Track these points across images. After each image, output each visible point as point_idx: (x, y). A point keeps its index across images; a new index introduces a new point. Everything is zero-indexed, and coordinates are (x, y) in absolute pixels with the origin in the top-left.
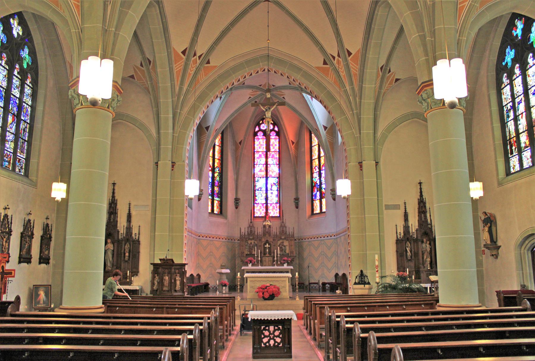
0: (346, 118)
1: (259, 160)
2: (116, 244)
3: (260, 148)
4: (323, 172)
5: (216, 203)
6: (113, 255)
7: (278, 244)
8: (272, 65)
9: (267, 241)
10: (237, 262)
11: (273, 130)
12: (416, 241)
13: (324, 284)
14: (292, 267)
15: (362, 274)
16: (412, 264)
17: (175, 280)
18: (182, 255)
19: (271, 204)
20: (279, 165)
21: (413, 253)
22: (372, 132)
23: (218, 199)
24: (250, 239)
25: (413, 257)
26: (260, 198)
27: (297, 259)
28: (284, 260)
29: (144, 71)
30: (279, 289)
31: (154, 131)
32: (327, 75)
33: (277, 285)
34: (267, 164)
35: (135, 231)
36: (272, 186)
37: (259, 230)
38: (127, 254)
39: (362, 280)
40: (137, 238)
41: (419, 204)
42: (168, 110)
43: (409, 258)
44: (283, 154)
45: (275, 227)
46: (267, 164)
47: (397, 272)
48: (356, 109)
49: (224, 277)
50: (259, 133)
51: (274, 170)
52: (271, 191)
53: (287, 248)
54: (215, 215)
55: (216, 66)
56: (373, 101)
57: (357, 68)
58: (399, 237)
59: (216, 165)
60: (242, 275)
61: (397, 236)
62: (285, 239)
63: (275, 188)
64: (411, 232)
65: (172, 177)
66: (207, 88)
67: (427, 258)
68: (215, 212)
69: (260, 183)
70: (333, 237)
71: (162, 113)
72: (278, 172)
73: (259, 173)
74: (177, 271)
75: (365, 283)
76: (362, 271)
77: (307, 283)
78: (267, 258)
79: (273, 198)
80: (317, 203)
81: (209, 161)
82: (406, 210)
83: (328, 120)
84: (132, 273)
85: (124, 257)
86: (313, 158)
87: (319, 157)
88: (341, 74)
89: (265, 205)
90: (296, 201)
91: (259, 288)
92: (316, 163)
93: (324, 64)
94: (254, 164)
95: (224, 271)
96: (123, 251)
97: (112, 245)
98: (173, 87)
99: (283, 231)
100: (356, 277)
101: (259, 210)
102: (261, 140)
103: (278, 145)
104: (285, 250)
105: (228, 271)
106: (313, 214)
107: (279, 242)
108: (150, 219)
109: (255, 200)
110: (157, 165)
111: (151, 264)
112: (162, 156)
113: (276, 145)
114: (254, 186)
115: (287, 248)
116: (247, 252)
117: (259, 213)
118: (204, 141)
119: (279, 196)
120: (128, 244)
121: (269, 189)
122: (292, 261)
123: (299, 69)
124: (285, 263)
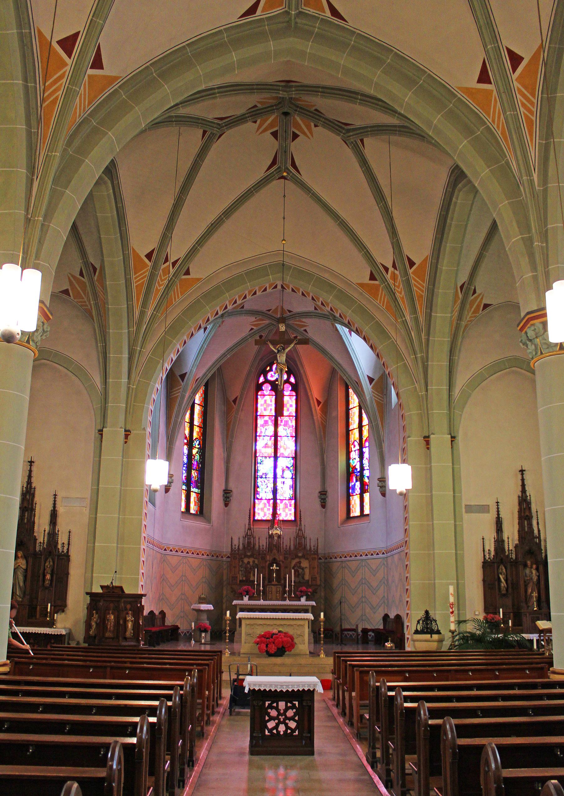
1: (263, 430)
3: (265, 410)
5: (193, 496)
6: (25, 577)
7: (293, 565)
9: (275, 559)
10: (225, 592)
12: (515, 563)
13: (365, 631)
14: (314, 603)
15: (427, 618)
16: (509, 601)
17: (125, 621)
19: (282, 500)
21: (509, 582)
22: (445, 388)
23: (196, 490)
25: (510, 590)
28: (301, 591)
30: (292, 638)
31: (97, 380)
33: (291, 632)
34: (276, 435)
35: (62, 539)
36: (283, 471)
38: (48, 577)
39: (428, 625)
40: (65, 551)
43: (504, 592)
46: (276, 435)
47: (485, 615)
48: (421, 351)
49: (204, 616)
50: (265, 385)
51: (288, 446)
52: (283, 480)
53: (307, 571)
55: (198, 280)
57: (423, 287)
58: (487, 557)
59: (195, 435)
60: (233, 615)
61: (484, 556)
62: (303, 557)
63: (288, 474)
64: (507, 549)
65: (125, 453)
67: (532, 593)
68: (192, 511)
69: (265, 467)
70: (381, 555)
72: (294, 448)
73: (264, 450)
75: (431, 632)
76: (427, 612)
78: (274, 588)
79: (285, 491)
80: (355, 500)
82: (498, 514)
84: (55, 606)
86: (351, 427)
87: (360, 427)
88: (398, 295)
89: (272, 501)
90: (323, 497)
91: (261, 636)
92: (355, 436)
93: (480, 81)
94: (256, 436)
95: (204, 607)
96: (41, 571)
97: (24, 562)
98: (130, 310)
100: (418, 622)
101: (262, 509)
102: (267, 398)
104: (304, 574)
105: (210, 607)
106: (349, 517)
107: (294, 562)
109: (256, 492)
110: (102, 435)
112: (109, 420)
114: (256, 471)
115: (307, 571)
116: (240, 577)
118: (176, 397)
119: (294, 487)
122: (315, 592)
123: (332, 287)
124: (302, 596)
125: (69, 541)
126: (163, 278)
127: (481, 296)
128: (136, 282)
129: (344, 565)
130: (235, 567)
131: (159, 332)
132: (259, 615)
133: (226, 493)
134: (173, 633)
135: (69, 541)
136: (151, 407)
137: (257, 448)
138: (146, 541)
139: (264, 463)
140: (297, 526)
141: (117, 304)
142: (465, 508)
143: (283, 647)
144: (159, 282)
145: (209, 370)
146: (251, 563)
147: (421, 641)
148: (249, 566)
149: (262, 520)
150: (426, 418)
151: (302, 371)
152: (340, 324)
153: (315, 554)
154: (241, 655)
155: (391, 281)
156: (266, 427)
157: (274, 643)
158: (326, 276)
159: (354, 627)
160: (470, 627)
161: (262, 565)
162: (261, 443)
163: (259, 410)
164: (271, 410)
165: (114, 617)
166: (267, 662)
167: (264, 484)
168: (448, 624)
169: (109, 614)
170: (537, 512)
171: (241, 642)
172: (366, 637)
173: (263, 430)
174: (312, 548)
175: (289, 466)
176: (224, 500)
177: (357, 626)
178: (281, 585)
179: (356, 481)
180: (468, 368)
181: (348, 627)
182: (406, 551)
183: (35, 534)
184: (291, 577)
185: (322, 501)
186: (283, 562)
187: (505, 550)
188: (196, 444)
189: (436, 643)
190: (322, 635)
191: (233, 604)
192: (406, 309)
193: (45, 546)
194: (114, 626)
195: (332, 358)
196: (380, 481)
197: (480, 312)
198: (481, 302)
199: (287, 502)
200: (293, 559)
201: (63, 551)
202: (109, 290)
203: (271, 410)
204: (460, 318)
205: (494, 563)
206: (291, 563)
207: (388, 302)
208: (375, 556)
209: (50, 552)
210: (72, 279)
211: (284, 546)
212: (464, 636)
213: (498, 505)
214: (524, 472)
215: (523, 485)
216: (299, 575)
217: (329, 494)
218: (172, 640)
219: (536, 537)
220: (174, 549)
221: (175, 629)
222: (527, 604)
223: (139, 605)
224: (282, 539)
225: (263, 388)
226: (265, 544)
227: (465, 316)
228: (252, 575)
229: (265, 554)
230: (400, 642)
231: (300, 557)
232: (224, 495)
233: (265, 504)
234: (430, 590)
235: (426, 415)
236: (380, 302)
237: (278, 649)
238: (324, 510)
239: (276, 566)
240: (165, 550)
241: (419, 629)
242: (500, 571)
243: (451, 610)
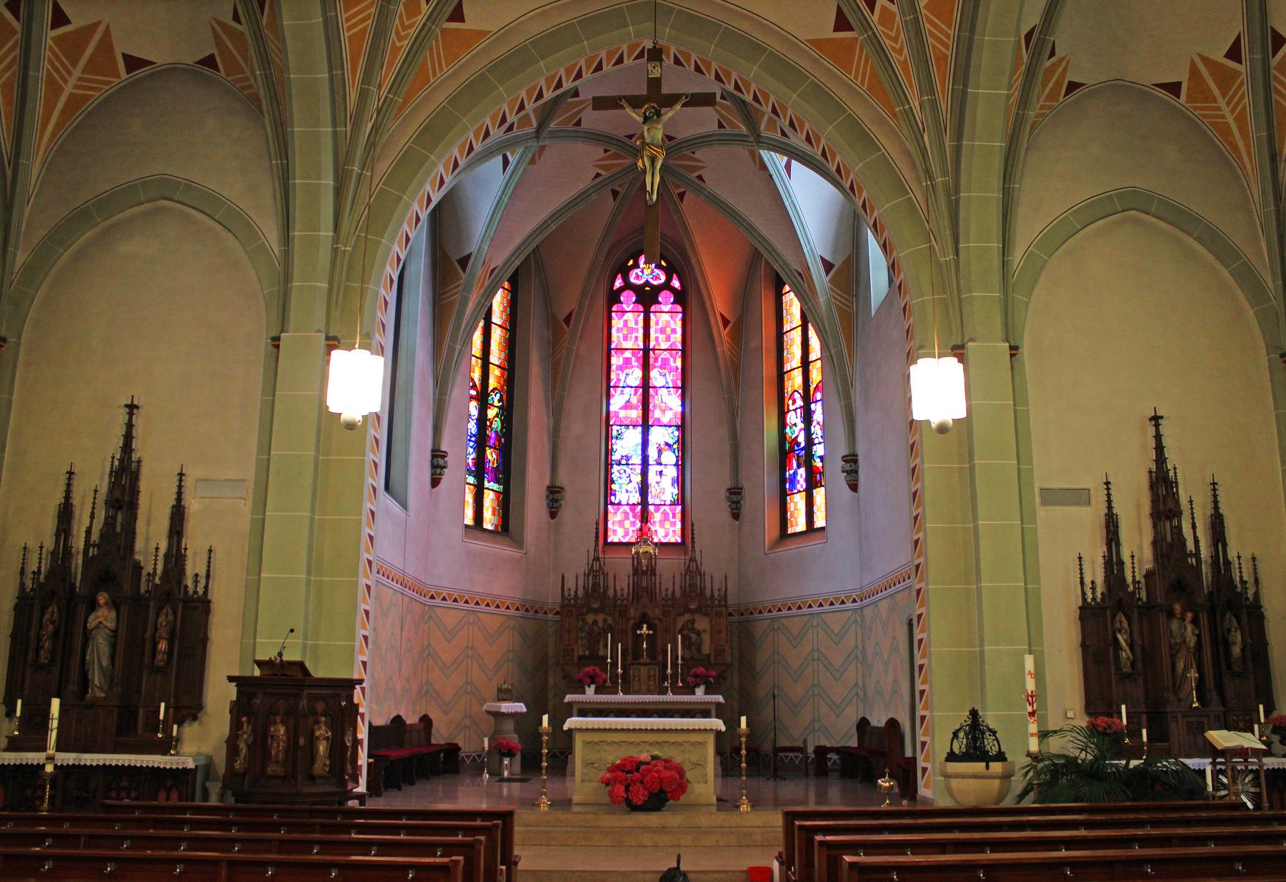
0: (909, 201)
2: (124, 609)
3: (625, 338)
4: (817, 408)
5: (489, 499)
6: (114, 646)
7: (679, 627)
8: (667, 37)
9: (644, 615)
10: (551, 680)
11: (667, 286)
12: (1149, 609)
13: (821, 751)
14: (720, 698)
15: (975, 727)
17: (312, 741)
18: (350, 652)
19: (658, 506)
20: (684, 389)
21: (1138, 649)
22: (996, 245)
23: (495, 486)
24: (591, 610)
25: (1139, 666)
26: (625, 487)
27: (736, 673)
28: (696, 676)
29: (242, 34)
30: (680, 771)
31: (272, 236)
32: (846, 67)
33: (678, 758)
34: (646, 385)
35: (194, 565)
36: (660, 452)
37: (620, 569)
38: (163, 645)
39: (975, 743)
40: (200, 590)
41: (1152, 487)
42: (319, 164)
44: (696, 358)
45: (669, 568)
46: (646, 385)
47: (1087, 719)
48: (945, 174)
49: (509, 726)
50: (626, 293)
51: (669, 404)
52: (659, 468)
53: (706, 638)
54: (486, 535)
55: (483, 34)
56: (999, 144)
57: (948, 37)
58: (1089, 596)
59: (493, 383)
60: (557, 722)
61: (1084, 594)
62: (698, 610)
63: (669, 458)
64: (1129, 579)
66: (454, 100)
67: (1186, 669)
68: (488, 525)
69: (627, 443)
70: (849, 605)
71: (298, 174)
72: (680, 409)
73: (622, 413)
74: (320, 706)
75: (985, 757)
76: (974, 713)
77: (767, 747)
78: (643, 670)
79: (664, 488)
80: (797, 503)
81: (471, 370)
82: (1110, 507)
83: (836, 244)
84: (176, 709)
85: (37, 652)
86: (787, 367)
87: (806, 363)
88: (894, 57)
90: (735, 498)
91: (614, 769)
92: (795, 381)
94: (609, 387)
95: (506, 707)
97: (113, 614)
98: (337, 87)
100: (955, 735)
101: (621, 524)
102: (629, 316)
103: (679, 331)
104: (700, 644)
105: (520, 707)
107: (681, 621)
108: (248, 526)
109: (609, 492)
110: (277, 347)
111: (231, 679)
112: (293, 314)
113: (674, 331)
114: (609, 452)
115: (706, 638)
116: (580, 650)
117: (620, 532)
118: (452, 303)
119: (680, 481)
120: (168, 609)
121: (651, 461)
122: (721, 677)
123: (756, 48)
125: (208, 571)
126: (407, 23)
127: (1064, 63)
128: (349, 29)
131: (403, 135)
132: (617, 723)
133: (552, 492)
134: (446, 762)
135: (208, 571)
136: (383, 292)
137: (612, 409)
138: (375, 570)
139: (625, 436)
140: (686, 553)
141: (306, 69)
142: (1041, 496)
143: (661, 791)
144: (397, 31)
145: (515, 253)
146: (601, 624)
147: (964, 776)
150: (957, 310)
151: (693, 261)
152: (769, 149)
153: (720, 606)
154: (575, 809)
155: (879, 27)
157: (642, 782)
158: (745, 26)
159: (800, 744)
160: (1056, 745)
161: (624, 628)
162: (617, 402)
163: (614, 337)
165: (287, 731)
166: (629, 823)
167: (624, 476)
168: (1022, 742)
169: (275, 723)
170: (1191, 501)
171: (573, 774)
172: (820, 764)
173: (622, 377)
174: (716, 593)
175: (671, 442)
177: (805, 741)
179: (799, 467)
180: (1049, 195)
181: (787, 743)
182: (917, 587)
183: (137, 557)
184: (676, 650)
186: (660, 620)
187: (1124, 580)
188: (495, 399)
189: (997, 782)
190: (744, 765)
191: (566, 700)
192: (911, 86)
193: (157, 581)
194: (287, 750)
195: (751, 229)
196: (846, 461)
197: (1061, 99)
198: (1063, 75)
200: (681, 614)
201: (196, 592)
202: (289, 41)
203: (636, 338)
204: (1024, 103)
205: (1104, 609)
206: (675, 621)
207: (873, 74)
208: (837, 606)
209: (168, 595)
210: (218, 29)
211: (663, 589)
212: (1054, 764)
213: (1108, 489)
214: (1160, 421)
215: (1159, 448)
216: (691, 644)
218: (446, 771)
219: (1191, 555)
220: (450, 596)
221: (452, 750)
222: (1176, 694)
223: (343, 703)
226: (626, 588)
227: (1036, 94)
230: (907, 775)
233: (626, 514)
234: (974, 669)
235: (957, 303)
236: (856, 78)
237: (651, 794)
239: (648, 629)
240: (432, 597)
241: (956, 750)
242: (1118, 625)
243: (1030, 709)
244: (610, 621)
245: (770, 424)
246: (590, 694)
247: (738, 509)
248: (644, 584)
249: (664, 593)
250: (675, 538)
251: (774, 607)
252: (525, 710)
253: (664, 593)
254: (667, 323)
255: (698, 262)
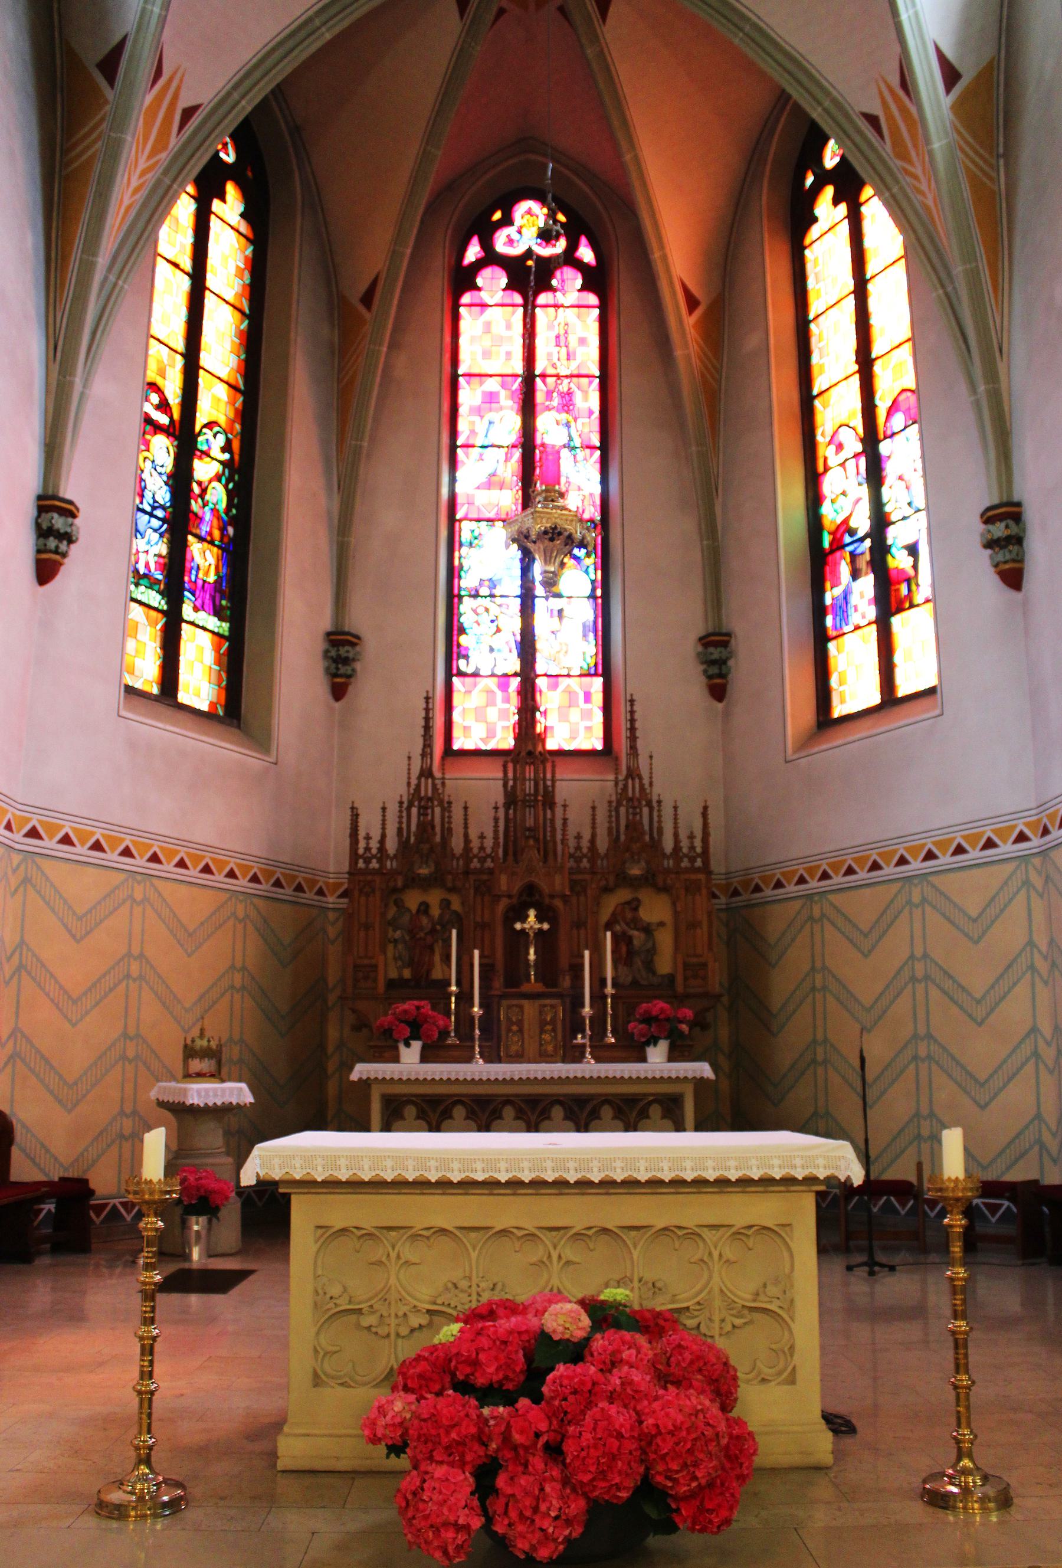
1: (481, 426)
3: (486, 354)
7: (605, 916)
9: (530, 889)
10: (333, 1034)
11: (569, 258)
14: (704, 1069)
24: (414, 882)
44: (629, 384)
53: (665, 940)
59: (204, 414)
62: (650, 880)
70: (1007, 848)
72: (597, 490)
78: (530, 1009)
89: (515, 682)
90: (716, 653)
94: (453, 448)
99: (633, 827)
101: (480, 714)
104: (652, 951)
106: (825, 721)
107: (611, 903)
109: (453, 651)
113: (582, 341)
114: (453, 573)
115: (665, 940)
122: (700, 1023)
124: (654, 1041)
129: (816, 912)
130: (367, 927)
137: (459, 488)
143: (647, 1489)
146: (435, 912)
148: (425, 921)
149: (477, 753)
156: (490, 416)
157: (554, 1451)
164: (508, 354)
173: (481, 426)
176: (327, 670)
178: (560, 996)
179: (855, 575)
184: (600, 964)
185: (714, 670)
186: (565, 899)
188: (213, 443)
191: (354, 1076)
199: (575, 684)
200: (607, 890)
203: (508, 354)
216: (631, 953)
217: (741, 645)
218: (58, 1248)
224: (559, 811)
225: (479, 282)
226: (489, 834)
228: (437, 958)
229: (491, 872)
231: (634, 883)
232: (326, 652)
233: (489, 692)
237: (596, 1509)
238: (720, 706)
239: (540, 919)
244: (456, 905)
245: (790, 497)
246: (410, 1063)
247: (722, 676)
248: (530, 822)
249: (572, 843)
250: (594, 741)
251: (811, 871)
252: (248, 1098)
253: (572, 843)
254: (571, 324)
255: (637, 160)
